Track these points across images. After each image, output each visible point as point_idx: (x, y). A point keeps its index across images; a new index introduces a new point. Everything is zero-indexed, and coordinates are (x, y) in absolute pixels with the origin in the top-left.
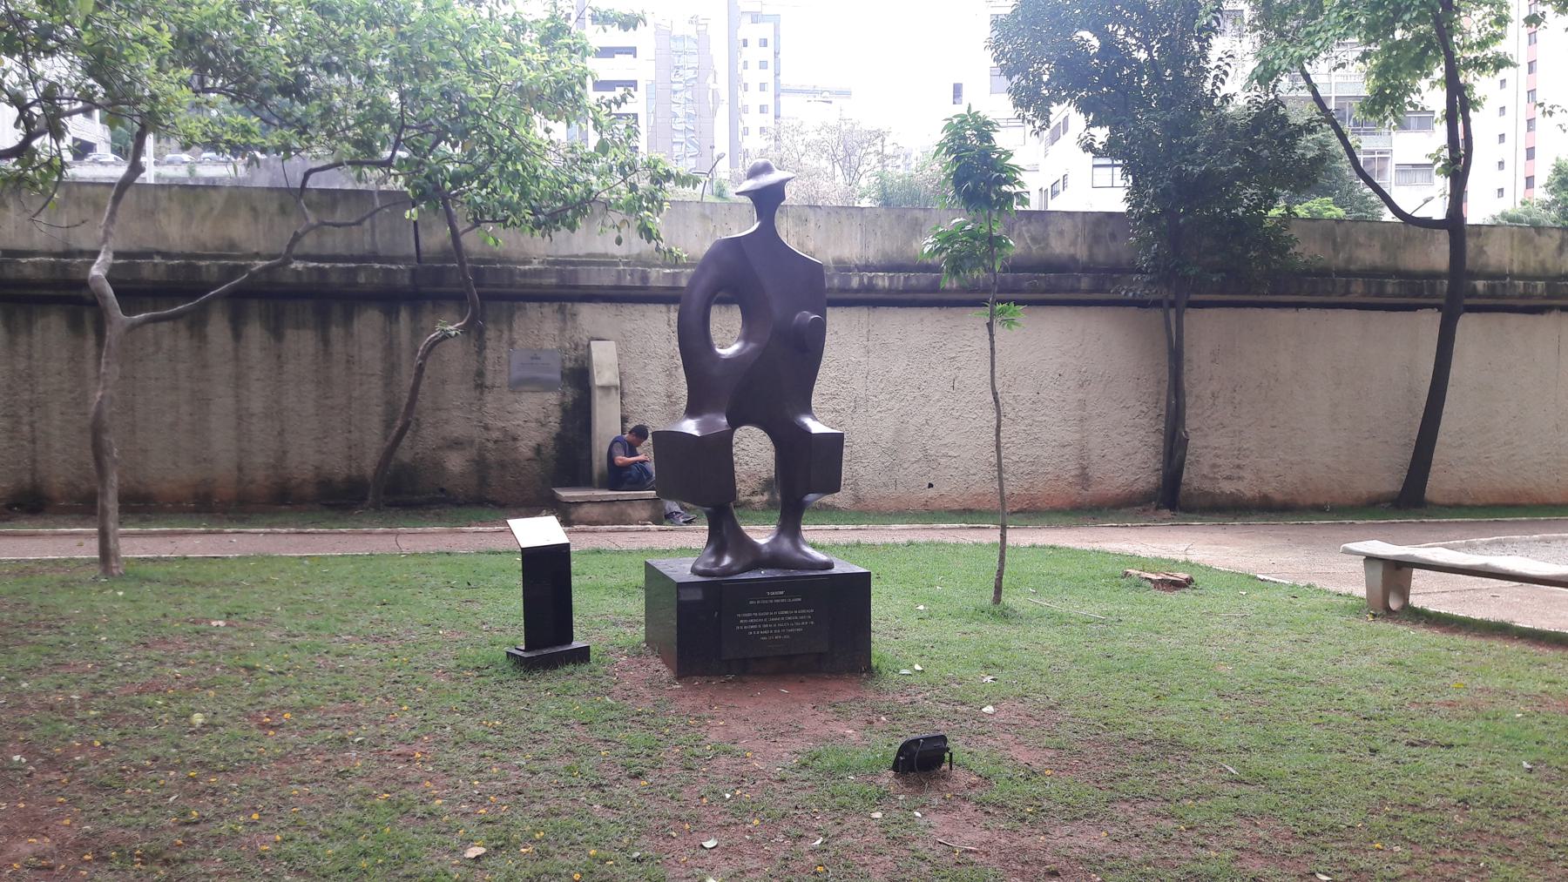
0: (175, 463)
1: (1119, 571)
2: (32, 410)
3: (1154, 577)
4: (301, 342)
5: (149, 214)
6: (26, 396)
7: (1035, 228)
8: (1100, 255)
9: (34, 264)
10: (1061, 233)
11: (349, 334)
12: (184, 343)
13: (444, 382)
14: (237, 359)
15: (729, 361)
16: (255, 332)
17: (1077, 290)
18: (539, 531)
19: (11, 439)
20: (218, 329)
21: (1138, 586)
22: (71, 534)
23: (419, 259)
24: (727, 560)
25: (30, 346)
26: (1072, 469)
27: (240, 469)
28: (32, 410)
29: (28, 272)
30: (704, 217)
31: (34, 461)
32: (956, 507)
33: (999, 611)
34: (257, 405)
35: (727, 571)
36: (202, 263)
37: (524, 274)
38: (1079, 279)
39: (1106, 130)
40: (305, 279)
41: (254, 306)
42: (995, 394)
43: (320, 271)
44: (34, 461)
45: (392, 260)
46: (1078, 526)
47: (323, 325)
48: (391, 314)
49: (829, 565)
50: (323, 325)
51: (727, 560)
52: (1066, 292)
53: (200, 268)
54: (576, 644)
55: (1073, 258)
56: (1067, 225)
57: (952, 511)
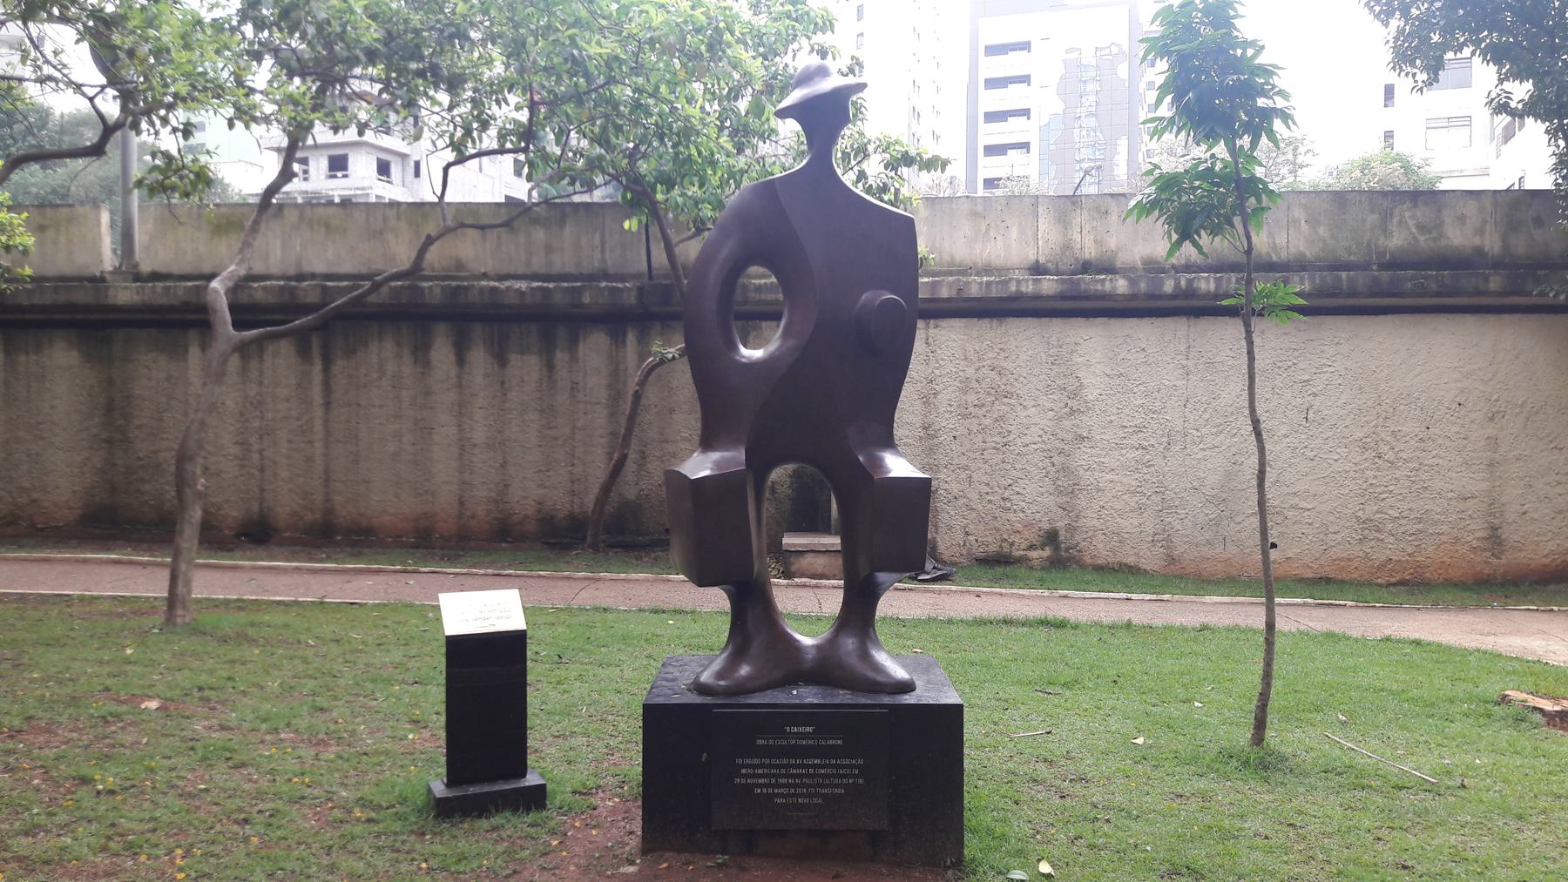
0: (397, 495)
1: (1493, 689)
2: (261, 438)
3: (1548, 706)
4: (525, 367)
5: (377, 234)
6: (256, 424)
7: (1423, 213)
8: (1520, 246)
9: (264, 288)
10: (1462, 219)
11: (574, 359)
12: (407, 368)
13: (672, 411)
14: (460, 385)
15: (753, 366)
16: (479, 357)
17: (1486, 293)
18: (480, 608)
19: (243, 467)
20: (442, 353)
21: (1519, 720)
22: (270, 568)
23: (650, 277)
24: (744, 670)
25: (262, 373)
26: (1476, 530)
27: (461, 503)
28: (261, 438)
29: (259, 296)
30: (975, 214)
31: (262, 490)
32: (1311, 575)
33: (1260, 760)
34: (479, 435)
35: (742, 689)
36: (425, 284)
37: (759, 289)
38: (1486, 279)
39: (1528, 86)
40: (528, 300)
41: (478, 330)
42: (1256, 423)
43: (494, 289)
44: (262, 490)
45: (622, 278)
46: (1479, 606)
47: (547, 349)
48: (618, 338)
49: (907, 687)
50: (547, 349)
51: (744, 670)
52: (1470, 294)
53: (423, 289)
54: (532, 779)
55: (1479, 251)
56: (1470, 209)
57: (1302, 580)
